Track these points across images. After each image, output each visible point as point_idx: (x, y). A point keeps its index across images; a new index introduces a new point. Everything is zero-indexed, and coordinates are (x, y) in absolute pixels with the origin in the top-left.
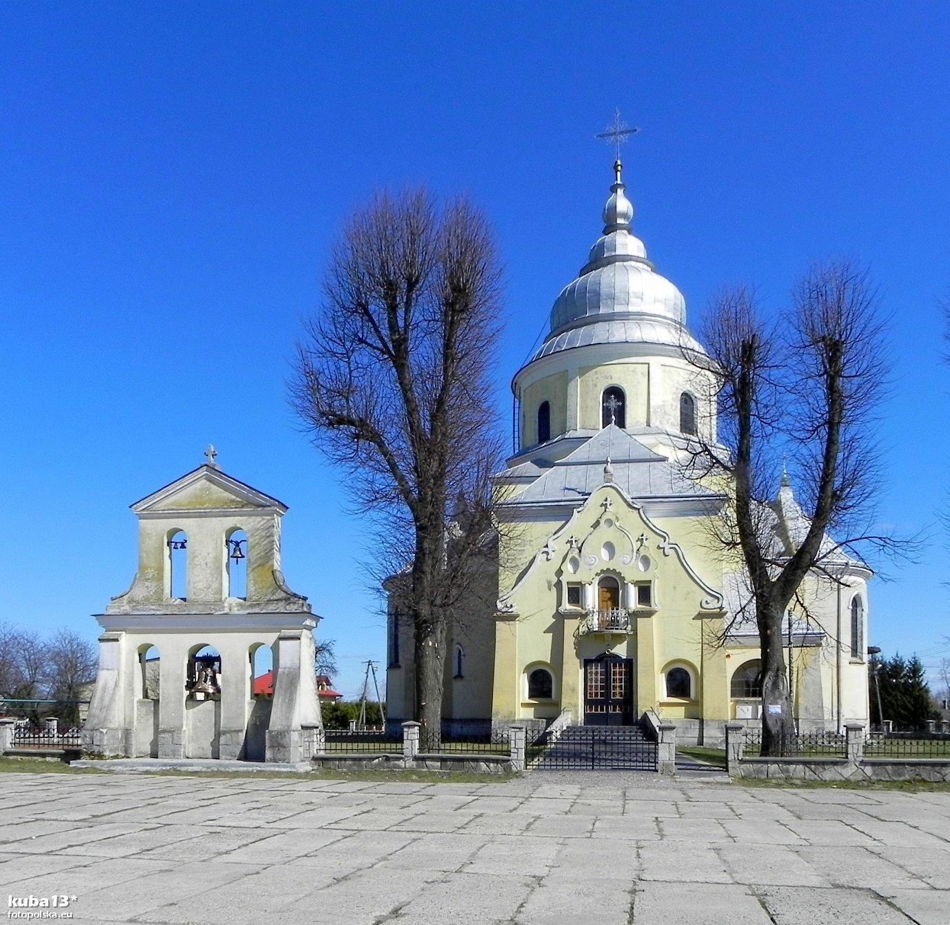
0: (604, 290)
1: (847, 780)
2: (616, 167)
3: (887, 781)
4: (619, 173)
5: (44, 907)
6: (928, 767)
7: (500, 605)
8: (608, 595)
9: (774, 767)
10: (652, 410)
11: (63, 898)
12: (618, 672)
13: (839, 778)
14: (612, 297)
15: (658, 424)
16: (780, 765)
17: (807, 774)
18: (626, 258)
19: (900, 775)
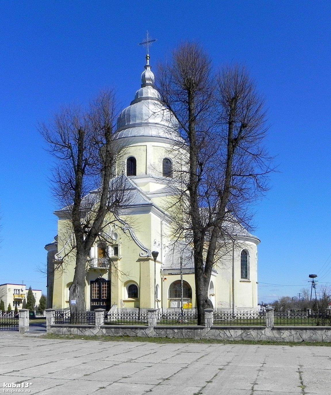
0: (132, 113)
1: (96, 336)
2: (147, 57)
3: (112, 336)
4: (148, 60)
5: (19, 387)
6: (129, 330)
7: (56, 257)
8: (102, 251)
9: (65, 329)
10: (147, 167)
11: (26, 384)
12: (104, 286)
13: (92, 334)
14: (135, 116)
15: (150, 173)
16: (67, 328)
17: (79, 332)
18: (147, 98)
19: (117, 334)
